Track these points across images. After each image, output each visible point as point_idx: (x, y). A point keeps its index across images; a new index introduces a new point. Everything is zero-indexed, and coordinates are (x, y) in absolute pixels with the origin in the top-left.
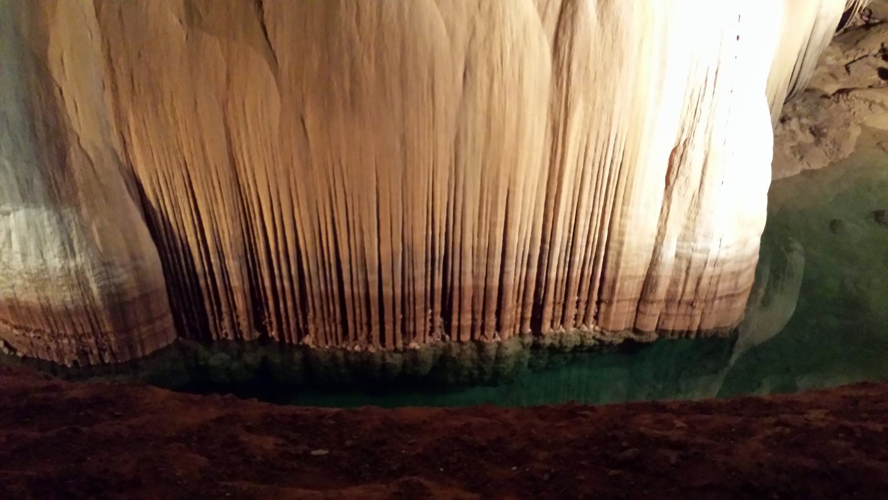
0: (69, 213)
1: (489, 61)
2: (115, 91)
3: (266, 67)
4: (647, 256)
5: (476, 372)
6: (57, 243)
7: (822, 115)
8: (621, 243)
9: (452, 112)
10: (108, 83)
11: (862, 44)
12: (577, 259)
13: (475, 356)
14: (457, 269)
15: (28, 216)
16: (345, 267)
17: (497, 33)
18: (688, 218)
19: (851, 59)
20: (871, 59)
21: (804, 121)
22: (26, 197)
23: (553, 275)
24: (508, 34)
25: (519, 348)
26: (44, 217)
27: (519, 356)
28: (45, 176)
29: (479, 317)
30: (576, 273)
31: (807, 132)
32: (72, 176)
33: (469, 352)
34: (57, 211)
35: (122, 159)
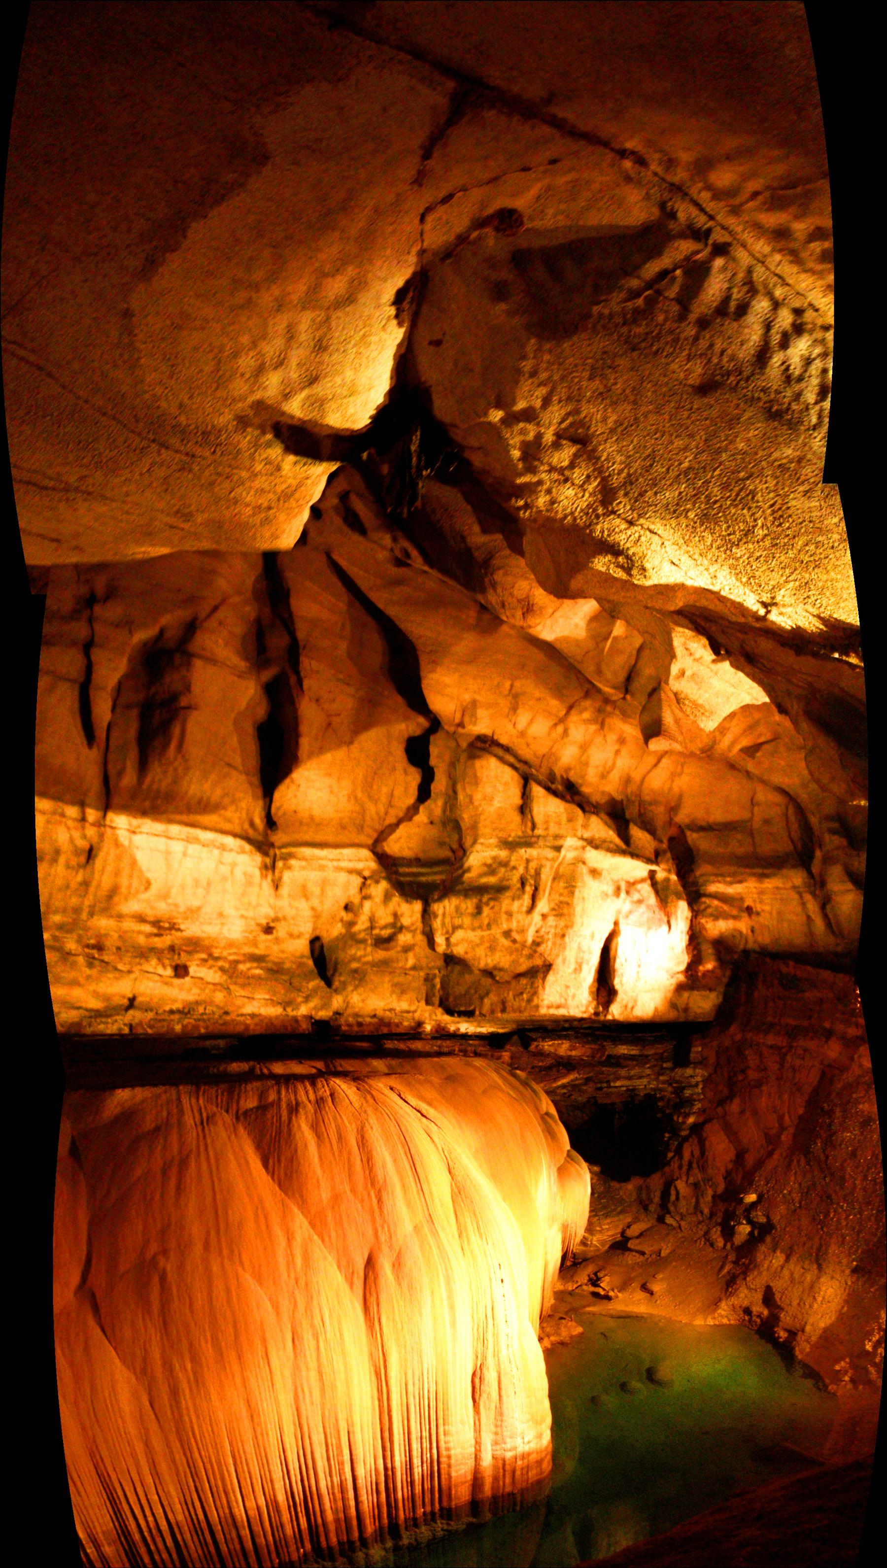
1: (313, 1326)
17: (315, 1302)
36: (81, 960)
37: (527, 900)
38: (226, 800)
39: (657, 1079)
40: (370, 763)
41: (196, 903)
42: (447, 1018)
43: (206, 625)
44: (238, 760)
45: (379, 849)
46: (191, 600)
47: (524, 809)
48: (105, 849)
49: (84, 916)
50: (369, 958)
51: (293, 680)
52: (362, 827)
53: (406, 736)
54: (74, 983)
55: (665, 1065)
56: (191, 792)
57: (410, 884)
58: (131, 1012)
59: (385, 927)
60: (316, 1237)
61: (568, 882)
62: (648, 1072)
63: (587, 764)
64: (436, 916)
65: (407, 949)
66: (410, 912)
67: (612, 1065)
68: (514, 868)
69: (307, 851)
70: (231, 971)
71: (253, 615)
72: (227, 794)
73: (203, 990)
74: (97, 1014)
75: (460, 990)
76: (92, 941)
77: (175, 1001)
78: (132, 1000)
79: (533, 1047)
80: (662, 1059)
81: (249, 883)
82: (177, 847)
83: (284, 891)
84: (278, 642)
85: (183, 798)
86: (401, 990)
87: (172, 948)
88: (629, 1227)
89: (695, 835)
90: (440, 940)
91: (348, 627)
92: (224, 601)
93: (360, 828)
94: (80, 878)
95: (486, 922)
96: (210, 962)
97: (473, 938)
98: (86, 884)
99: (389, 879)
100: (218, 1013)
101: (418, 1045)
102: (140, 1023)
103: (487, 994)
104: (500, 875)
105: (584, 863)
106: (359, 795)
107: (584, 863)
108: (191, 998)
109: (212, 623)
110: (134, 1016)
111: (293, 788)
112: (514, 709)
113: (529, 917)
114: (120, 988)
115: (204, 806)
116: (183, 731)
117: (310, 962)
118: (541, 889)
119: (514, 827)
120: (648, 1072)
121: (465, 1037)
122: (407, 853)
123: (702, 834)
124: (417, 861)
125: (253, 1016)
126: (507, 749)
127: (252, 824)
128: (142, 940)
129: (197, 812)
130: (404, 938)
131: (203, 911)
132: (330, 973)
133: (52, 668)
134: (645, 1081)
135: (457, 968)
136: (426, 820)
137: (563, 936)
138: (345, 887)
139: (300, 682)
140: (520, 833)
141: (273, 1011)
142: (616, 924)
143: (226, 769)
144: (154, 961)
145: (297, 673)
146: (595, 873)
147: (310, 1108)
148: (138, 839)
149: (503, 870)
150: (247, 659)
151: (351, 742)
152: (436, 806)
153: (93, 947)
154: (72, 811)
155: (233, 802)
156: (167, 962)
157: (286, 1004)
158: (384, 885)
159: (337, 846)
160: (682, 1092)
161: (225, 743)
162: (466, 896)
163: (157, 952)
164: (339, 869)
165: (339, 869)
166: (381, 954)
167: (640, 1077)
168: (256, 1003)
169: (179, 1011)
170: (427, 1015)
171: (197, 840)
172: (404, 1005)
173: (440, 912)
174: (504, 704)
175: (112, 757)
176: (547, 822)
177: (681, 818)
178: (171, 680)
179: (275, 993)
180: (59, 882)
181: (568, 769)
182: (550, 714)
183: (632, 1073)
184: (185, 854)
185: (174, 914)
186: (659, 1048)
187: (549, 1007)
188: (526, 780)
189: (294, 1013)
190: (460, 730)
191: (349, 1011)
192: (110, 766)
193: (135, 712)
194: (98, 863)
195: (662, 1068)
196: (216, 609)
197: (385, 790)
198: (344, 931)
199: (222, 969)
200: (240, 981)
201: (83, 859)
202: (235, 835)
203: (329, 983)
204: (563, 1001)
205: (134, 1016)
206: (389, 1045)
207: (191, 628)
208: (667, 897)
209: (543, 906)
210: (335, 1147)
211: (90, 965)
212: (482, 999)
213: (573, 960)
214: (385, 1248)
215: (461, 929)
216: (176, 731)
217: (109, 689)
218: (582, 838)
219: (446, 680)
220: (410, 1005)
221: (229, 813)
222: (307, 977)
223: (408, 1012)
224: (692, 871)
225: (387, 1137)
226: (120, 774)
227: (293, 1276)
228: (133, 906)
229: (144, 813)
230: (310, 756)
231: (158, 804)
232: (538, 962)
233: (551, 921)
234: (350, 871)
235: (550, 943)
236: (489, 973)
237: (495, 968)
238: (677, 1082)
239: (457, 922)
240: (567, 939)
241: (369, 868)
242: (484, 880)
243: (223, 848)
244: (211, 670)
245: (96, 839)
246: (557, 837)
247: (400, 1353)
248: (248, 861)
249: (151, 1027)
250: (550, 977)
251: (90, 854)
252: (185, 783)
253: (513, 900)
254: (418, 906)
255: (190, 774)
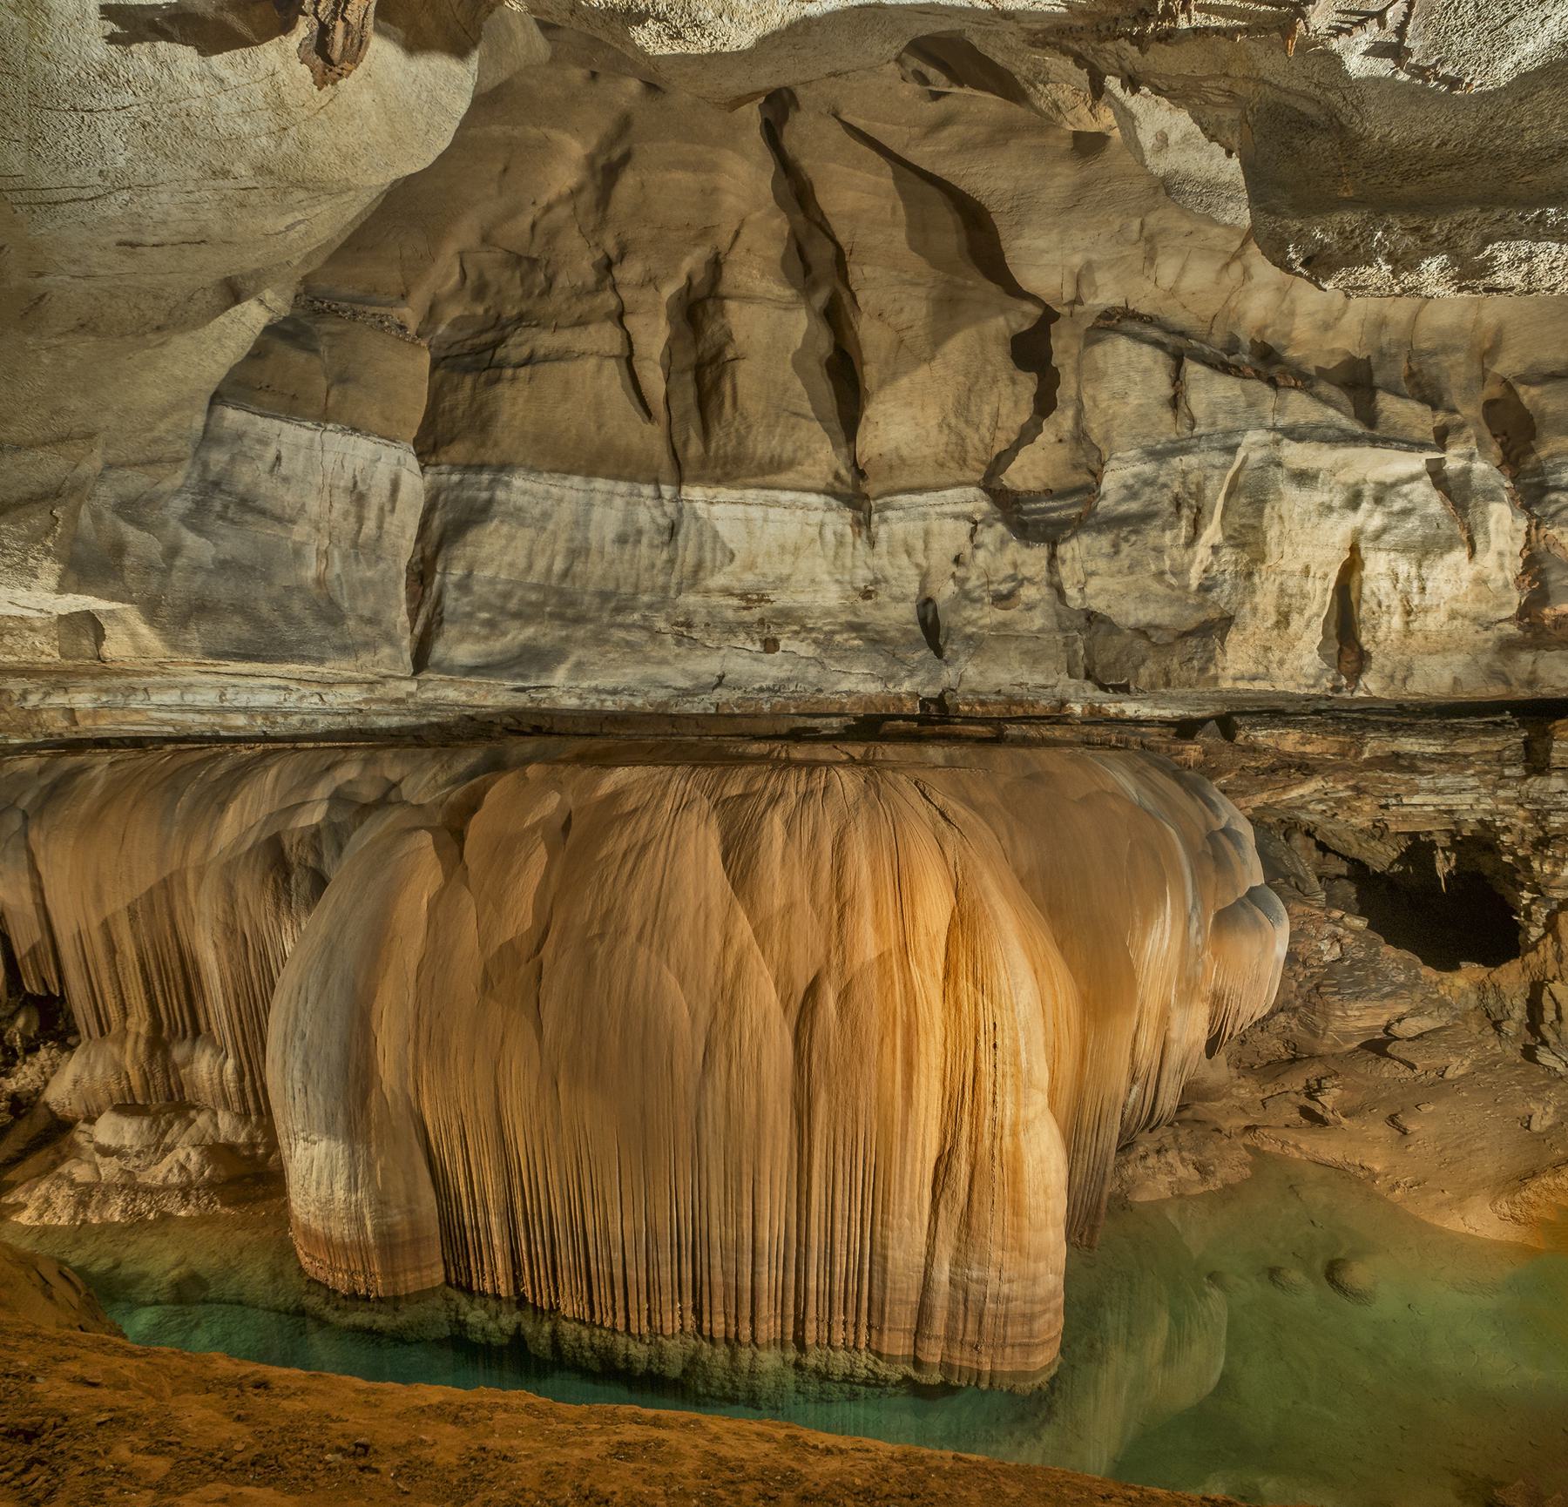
0: (361, 1150)
1: (728, 1045)
2: (417, 1044)
3: (532, 1032)
4: (916, 1279)
5: (729, 1385)
6: (345, 1176)
7: (1210, 1152)
8: (885, 1258)
9: (691, 1089)
10: (413, 1036)
11: (1281, 1080)
12: (838, 1269)
13: (727, 1365)
14: (705, 1261)
15: (328, 1147)
16: (591, 1239)
17: (737, 1019)
18: (959, 1239)
19: (1268, 1094)
20: (1292, 1096)
21: (1185, 1154)
22: (329, 1131)
23: (812, 1284)
24: (747, 1019)
25: (779, 1364)
26: (339, 1149)
27: (778, 1373)
28: (347, 1113)
29: (733, 1322)
30: (838, 1287)
31: (1191, 1167)
32: (368, 1115)
33: (721, 1358)
34: (352, 1146)
35: (414, 1105)
36: (669, 638)
37: (1184, 528)
38: (800, 454)
39: (1493, 795)
40: (961, 379)
41: (786, 571)
42: (1099, 694)
43: (731, 257)
44: (807, 407)
45: (995, 485)
46: (706, 232)
47: (1175, 402)
48: (685, 524)
49: (672, 594)
50: (987, 621)
51: (846, 298)
52: (965, 461)
53: (1009, 335)
54: (663, 662)
55: (1507, 772)
56: (759, 451)
57: (1036, 523)
58: (718, 690)
59: (1005, 580)
60: (756, 947)
61: (1251, 495)
62: (1472, 782)
63: (1292, 314)
64: (1064, 562)
65: (1030, 607)
66: (1033, 559)
67: (1402, 769)
68: (1165, 486)
69: (903, 499)
70: (825, 643)
71: (786, 229)
72: (800, 448)
73: (795, 665)
74: (685, 693)
75: (1109, 656)
76: (681, 619)
77: (766, 678)
78: (721, 678)
79: (1240, 738)
80: (1500, 760)
81: (840, 543)
82: (756, 513)
83: (882, 547)
84: (821, 254)
85: (753, 459)
86: (1034, 658)
87: (761, 622)
88: (1399, 1021)
89: (1534, 391)
90: (1071, 591)
91: (901, 212)
92: (742, 223)
93: (963, 462)
94: (665, 556)
95: (1127, 563)
96: (803, 635)
97: (1117, 587)
98: (671, 561)
99: (1006, 521)
100: (811, 690)
101: (1058, 732)
102: (727, 703)
103: (1144, 661)
104: (1144, 498)
105: (1279, 465)
106: (953, 421)
107: (1279, 465)
108: (783, 675)
109: (738, 253)
110: (722, 695)
111: (870, 428)
112: (1150, 258)
113: (1190, 552)
114: (707, 665)
115: (777, 465)
116: (734, 388)
117: (918, 629)
118: (1206, 511)
119: (1166, 427)
120: (1472, 782)
121: (1137, 722)
122: (1033, 485)
123: (1549, 387)
124: (1049, 493)
125: (849, 693)
126: (1150, 320)
127: (837, 476)
128: (730, 614)
129: (770, 473)
130: (1028, 593)
131: (793, 579)
132: (941, 641)
133: (595, 348)
134: (1469, 798)
135: (1103, 627)
136: (1053, 439)
137: (1250, 575)
138: (952, 536)
139: (854, 297)
140: (1173, 436)
141: (872, 688)
142: (1354, 549)
143: (793, 420)
144: (742, 636)
145: (848, 287)
146: (1303, 478)
147: (793, 799)
148: (716, 509)
149: (1148, 490)
150: (793, 285)
151: (933, 358)
152: (1063, 420)
153: (682, 625)
154: (648, 490)
155: (809, 454)
156: (756, 636)
157: (887, 679)
158: (1000, 528)
159: (938, 488)
160: (1545, 819)
161: (786, 390)
162: (1100, 532)
163: (745, 626)
164: (943, 515)
165: (943, 515)
166: (999, 615)
167: (1461, 791)
168: (852, 678)
169: (769, 689)
170: (1071, 690)
171: (777, 503)
172: (1039, 679)
173: (1069, 556)
174: (1136, 253)
175: (676, 428)
176: (1213, 414)
177: (1506, 365)
178: (712, 329)
179: (875, 666)
180: (645, 562)
181: (1261, 330)
182: (1212, 251)
183: (1441, 783)
184: (765, 520)
185: (763, 585)
186: (1494, 744)
187: (1235, 679)
188: (1178, 360)
189: (897, 689)
190: (1078, 308)
191: (963, 687)
192: (675, 439)
193: (689, 376)
194: (680, 538)
195: (1502, 777)
196: (737, 233)
197: (987, 409)
198: (956, 589)
199: (815, 641)
200: (835, 654)
201: (666, 537)
202: (818, 492)
203: (939, 652)
204: (1261, 669)
205: (722, 695)
206: (1013, 730)
207: (716, 265)
208: (1466, 500)
209: (1212, 533)
210: (804, 848)
211: (679, 643)
212: (1136, 668)
213: (1271, 609)
214: (834, 974)
215: (1094, 574)
216: (727, 388)
217: (657, 356)
218: (1274, 429)
219: (1041, 243)
220: (1047, 678)
221: (806, 468)
222: (914, 645)
223: (1045, 687)
224: (1532, 451)
225: (873, 839)
226: (685, 444)
227: (720, 983)
228: (718, 580)
229: (718, 482)
230: (882, 384)
231: (730, 469)
232: (1213, 614)
233: (1227, 555)
234: (956, 517)
235: (1227, 587)
236: (1142, 632)
237: (1150, 626)
238: (1534, 801)
239: (1091, 566)
240: (1256, 579)
241: (979, 510)
242: (1123, 508)
243: (806, 507)
244: (752, 309)
245: (675, 516)
246: (1229, 433)
247: (830, 1102)
248: (839, 521)
249: (738, 707)
250: (1233, 636)
251: (673, 530)
252: (751, 444)
253: (1163, 530)
254: (1041, 551)
255: (754, 432)
